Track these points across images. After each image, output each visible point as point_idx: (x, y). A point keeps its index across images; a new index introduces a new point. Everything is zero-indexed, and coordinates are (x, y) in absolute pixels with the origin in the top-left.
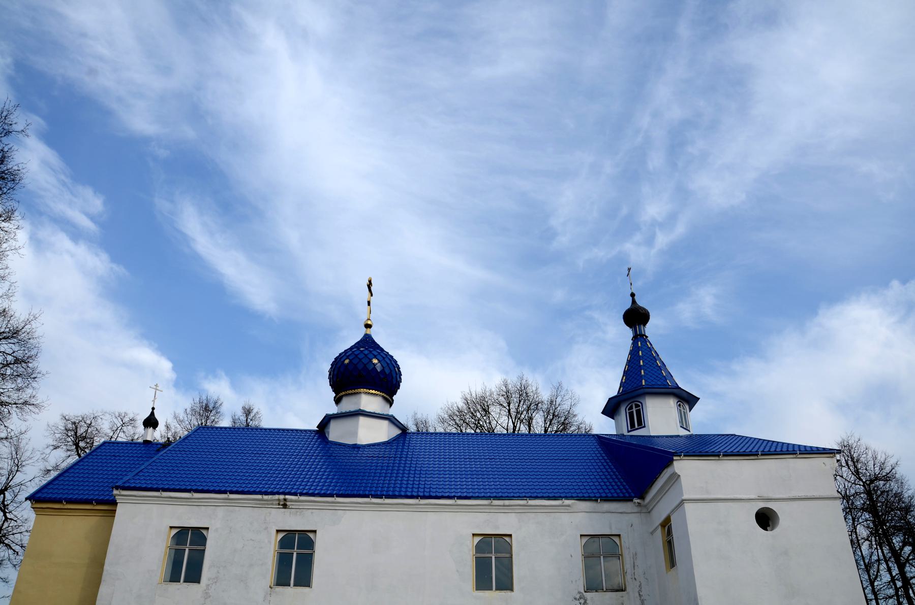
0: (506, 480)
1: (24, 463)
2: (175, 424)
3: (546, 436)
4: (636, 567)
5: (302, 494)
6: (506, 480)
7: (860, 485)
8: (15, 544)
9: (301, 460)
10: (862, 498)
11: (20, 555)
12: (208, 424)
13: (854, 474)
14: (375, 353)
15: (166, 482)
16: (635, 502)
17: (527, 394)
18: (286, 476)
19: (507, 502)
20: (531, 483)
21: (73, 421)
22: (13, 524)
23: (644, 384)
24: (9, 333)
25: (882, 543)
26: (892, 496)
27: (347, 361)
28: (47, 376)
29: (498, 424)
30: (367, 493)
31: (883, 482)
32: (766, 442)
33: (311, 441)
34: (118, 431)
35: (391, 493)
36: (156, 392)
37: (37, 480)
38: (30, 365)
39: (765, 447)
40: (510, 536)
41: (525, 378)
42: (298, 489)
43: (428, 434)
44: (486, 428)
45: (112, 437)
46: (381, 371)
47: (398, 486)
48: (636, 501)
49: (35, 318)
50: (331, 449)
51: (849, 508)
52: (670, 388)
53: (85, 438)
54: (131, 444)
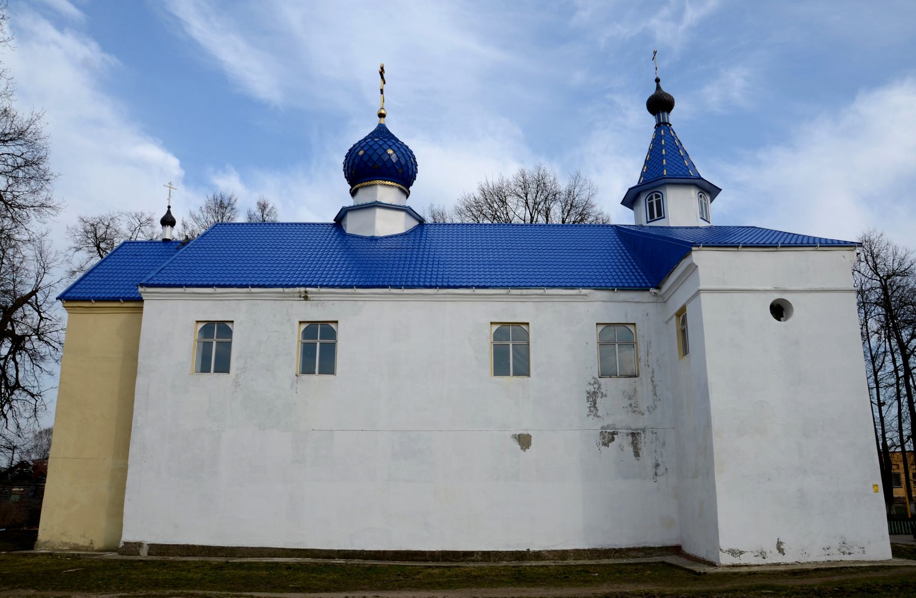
0: (523, 270)
1: (50, 266)
2: (191, 222)
3: (563, 226)
4: (650, 355)
5: (322, 286)
6: (523, 270)
7: (877, 280)
8: (53, 341)
9: (320, 253)
10: (877, 293)
11: (60, 352)
12: (225, 220)
13: (871, 269)
14: (390, 144)
15: (188, 279)
16: (651, 292)
17: (544, 183)
18: (301, 276)
19: (524, 291)
20: (549, 273)
21: (91, 222)
22: (48, 322)
23: (665, 173)
24: (14, 134)
25: (891, 336)
26: (908, 291)
27: (361, 153)
28: (59, 177)
29: (515, 215)
30: (386, 283)
31: (900, 277)
32: (786, 235)
33: (329, 234)
34: (137, 231)
35: (409, 284)
36: (170, 191)
37: (64, 281)
38: (41, 167)
39: (785, 239)
40: (528, 324)
41: (542, 167)
42: (318, 281)
43: (445, 225)
44: (503, 219)
45: (131, 237)
46: (396, 162)
47: (417, 276)
48: (653, 290)
49: (39, 118)
50: (349, 242)
51: (864, 303)
52: (693, 179)
53: (104, 239)
54: (151, 242)
